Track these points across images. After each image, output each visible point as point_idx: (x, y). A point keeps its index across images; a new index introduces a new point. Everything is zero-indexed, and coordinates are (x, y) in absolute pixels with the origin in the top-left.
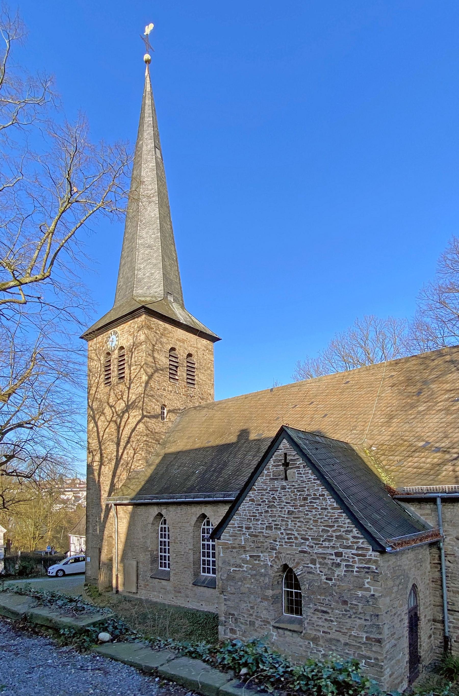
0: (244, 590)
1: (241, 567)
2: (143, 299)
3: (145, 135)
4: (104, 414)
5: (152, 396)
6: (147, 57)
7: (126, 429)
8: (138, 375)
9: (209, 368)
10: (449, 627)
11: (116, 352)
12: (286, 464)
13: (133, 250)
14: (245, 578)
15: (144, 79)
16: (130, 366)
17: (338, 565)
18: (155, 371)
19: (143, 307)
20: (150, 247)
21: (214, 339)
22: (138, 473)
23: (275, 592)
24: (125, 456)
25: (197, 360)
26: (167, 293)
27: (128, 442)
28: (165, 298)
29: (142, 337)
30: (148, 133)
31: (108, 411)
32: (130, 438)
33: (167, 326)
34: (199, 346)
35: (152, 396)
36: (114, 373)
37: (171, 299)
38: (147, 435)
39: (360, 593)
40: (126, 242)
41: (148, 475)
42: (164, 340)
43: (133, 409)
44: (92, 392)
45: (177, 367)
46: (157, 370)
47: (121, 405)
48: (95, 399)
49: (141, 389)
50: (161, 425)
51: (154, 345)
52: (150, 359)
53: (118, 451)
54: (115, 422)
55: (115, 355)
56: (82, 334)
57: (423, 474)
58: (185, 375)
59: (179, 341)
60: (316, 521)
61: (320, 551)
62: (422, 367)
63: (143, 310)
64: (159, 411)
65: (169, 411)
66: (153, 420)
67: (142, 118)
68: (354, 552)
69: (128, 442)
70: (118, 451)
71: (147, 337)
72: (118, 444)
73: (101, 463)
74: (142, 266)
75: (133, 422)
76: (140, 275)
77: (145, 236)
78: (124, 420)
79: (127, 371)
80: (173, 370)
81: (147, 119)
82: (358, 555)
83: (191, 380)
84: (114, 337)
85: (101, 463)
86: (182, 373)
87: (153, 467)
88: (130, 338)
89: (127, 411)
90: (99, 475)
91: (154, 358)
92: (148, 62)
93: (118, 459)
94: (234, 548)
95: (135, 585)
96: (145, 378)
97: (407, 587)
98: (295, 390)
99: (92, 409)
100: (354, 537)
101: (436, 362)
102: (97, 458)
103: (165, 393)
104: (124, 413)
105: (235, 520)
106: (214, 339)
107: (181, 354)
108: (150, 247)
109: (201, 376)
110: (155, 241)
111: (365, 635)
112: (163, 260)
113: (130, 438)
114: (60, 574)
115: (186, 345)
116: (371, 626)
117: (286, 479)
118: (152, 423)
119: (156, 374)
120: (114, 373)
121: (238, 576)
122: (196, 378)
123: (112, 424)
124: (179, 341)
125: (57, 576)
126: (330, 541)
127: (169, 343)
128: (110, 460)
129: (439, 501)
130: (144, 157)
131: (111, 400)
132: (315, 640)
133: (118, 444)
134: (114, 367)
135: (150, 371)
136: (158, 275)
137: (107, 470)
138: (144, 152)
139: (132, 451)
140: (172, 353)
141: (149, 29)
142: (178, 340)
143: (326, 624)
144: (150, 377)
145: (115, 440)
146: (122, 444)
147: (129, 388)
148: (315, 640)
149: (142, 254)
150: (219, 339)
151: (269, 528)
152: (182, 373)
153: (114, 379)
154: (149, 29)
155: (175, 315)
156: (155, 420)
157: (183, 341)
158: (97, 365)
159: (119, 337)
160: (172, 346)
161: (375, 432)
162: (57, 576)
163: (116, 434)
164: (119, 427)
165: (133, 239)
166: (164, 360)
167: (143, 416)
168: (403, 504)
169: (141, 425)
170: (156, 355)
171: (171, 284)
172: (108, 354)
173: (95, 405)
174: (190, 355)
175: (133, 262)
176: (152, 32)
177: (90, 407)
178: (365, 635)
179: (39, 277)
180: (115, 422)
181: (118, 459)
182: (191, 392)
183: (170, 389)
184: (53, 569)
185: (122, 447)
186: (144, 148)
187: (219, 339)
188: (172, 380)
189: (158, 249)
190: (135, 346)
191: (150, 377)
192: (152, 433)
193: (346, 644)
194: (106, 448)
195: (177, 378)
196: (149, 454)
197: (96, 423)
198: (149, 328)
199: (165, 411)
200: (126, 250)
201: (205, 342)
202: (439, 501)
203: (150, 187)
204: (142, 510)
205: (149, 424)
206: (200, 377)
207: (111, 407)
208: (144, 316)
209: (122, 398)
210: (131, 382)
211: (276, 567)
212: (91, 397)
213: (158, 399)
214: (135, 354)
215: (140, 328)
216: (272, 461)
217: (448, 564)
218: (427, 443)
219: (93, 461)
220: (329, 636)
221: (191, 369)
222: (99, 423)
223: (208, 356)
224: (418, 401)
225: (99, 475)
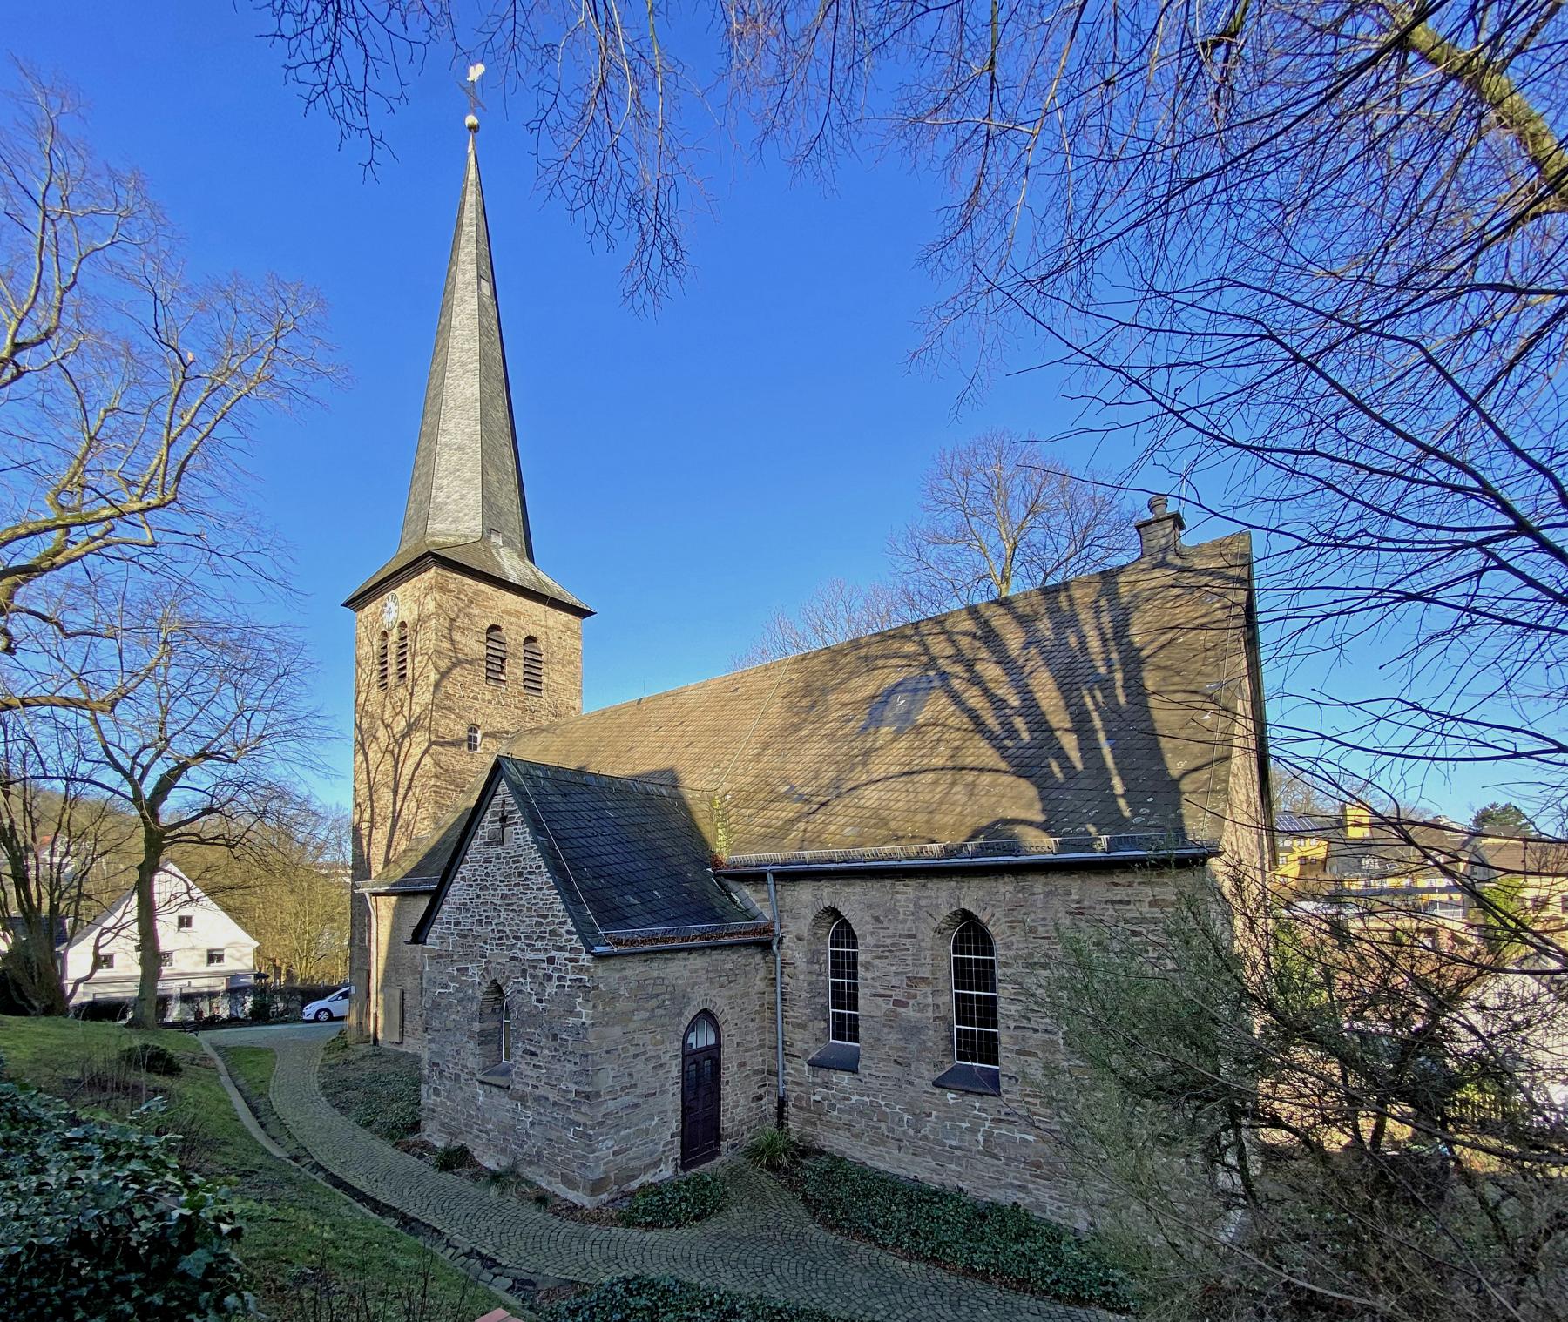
0: (450, 1024)
1: (447, 986)
2: (441, 540)
3: (462, 256)
4: (376, 738)
5: (450, 709)
6: (471, 120)
7: (407, 765)
8: (424, 670)
9: (572, 663)
10: (784, 1082)
11: (395, 630)
12: (503, 819)
13: (432, 452)
14: (451, 1005)
15: (467, 156)
16: (413, 656)
17: (550, 978)
18: (455, 665)
19: (429, 554)
20: (461, 448)
21: (582, 613)
22: (420, 840)
23: (485, 1025)
24: (405, 812)
25: (548, 647)
26: (489, 530)
27: (409, 788)
28: (485, 538)
29: (431, 606)
30: (468, 251)
31: (382, 733)
32: (411, 780)
33: (483, 587)
34: (551, 623)
35: (450, 709)
36: (392, 669)
37: (497, 540)
38: (436, 776)
39: (571, 1021)
40: (423, 440)
41: (432, 843)
42: (475, 611)
43: (417, 730)
44: (361, 700)
45: (503, 660)
46: (457, 663)
47: (400, 725)
48: (365, 713)
49: (427, 697)
50: (468, 759)
51: (453, 620)
52: (446, 645)
53: (395, 803)
54: (392, 752)
55: (394, 636)
56: (346, 599)
57: (775, 835)
58: (520, 673)
59: (509, 613)
60: (529, 909)
61: (532, 956)
62: (829, 666)
63: (430, 559)
64: (463, 734)
65: (485, 735)
66: (452, 750)
67: (459, 226)
68: (567, 955)
69: (409, 788)
70: (395, 803)
71: (439, 606)
72: (395, 792)
73: (372, 826)
74: (445, 482)
75: (417, 752)
76: (440, 497)
77: (453, 430)
78: (404, 749)
79: (409, 664)
80: (495, 667)
81: (466, 229)
82: (570, 960)
83: (532, 682)
84: (391, 604)
85: (372, 826)
86: (514, 670)
87: (442, 831)
88: (415, 607)
89: (408, 734)
90: (369, 844)
91: (452, 642)
92: (474, 128)
93: (396, 818)
94: (440, 957)
95: (398, 1030)
96: (434, 676)
97: (680, 1014)
98: (669, 700)
99: (361, 732)
100: (568, 932)
101: (849, 658)
102: (367, 816)
103: (476, 704)
104: (403, 737)
105: (444, 914)
106: (582, 613)
107: (513, 636)
108: (461, 448)
109: (555, 676)
110: (470, 439)
111: (573, 1088)
112: (484, 472)
113: (411, 780)
114: (324, 1016)
115: (522, 623)
116: (581, 1073)
117: (502, 843)
118: (448, 756)
119: (458, 670)
120: (392, 669)
121: (443, 1002)
122: (544, 678)
123: (388, 757)
124: (509, 613)
125: (316, 1020)
126: (543, 939)
127: (486, 617)
128: (385, 819)
129: (770, 877)
130: (458, 294)
131: (387, 715)
132: (523, 1099)
133: (395, 792)
134: (392, 658)
135: (444, 664)
136: (474, 498)
137: (380, 836)
138: (459, 285)
139: (414, 804)
140: (493, 635)
141: (476, 72)
142: (504, 611)
143: (534, 1073)
144: (444, 675)
145: (392, 784)
146: (401, 791)
147: (411, 694)
148: (523, 1099)
149: (445, 461)
150: (589, 613)
151: (480, 922)
152: (514, 670)
153: (392, 680)
154: (476, 72)
155: (500, 567)
156: (454, 750)
157: (517, 614)
158: (369, 650)
159: (400, 605)
160: (492, 622)
161: (740, 771)
162: (316, 1020)
163: (392, 774)
164: (397, 763)
165: (432, 437)
166: (474, 645)
167: (431, 743)
168: (732, 884)
169: (427, 760)
170: (457, 636)
171: (500, 514)
172: (385, 634)
173: (365, 724)
174: (531, 639)
175: (430, 474)
176: (481, 77)
177: (358, 727)
178: (573, 1088)
179: (154, 502)
180: (392, 752)
181: (396, 818)
182: (533, 701)
183: (488, 696)
184: (311, 1010)
185: (400, 797)
186: (459, 278)
187: (589, 613)
188: (492, 682)
189: (475, 452)
190: (422, 620)
191: (444, 675)
192: (445, 772)
193: (555, 1104)
194: (379, 798)
195: (502, 677)
196: (441, 809)
197: (366, 755)
198: (443, 589)
199: (479, 735)
200: (422, 454)
201: (564, 617)
202: (770, 877)
203: (466, 346)
204: (410, 901)
205: (442, 758)
206: (551, 676)
207: (386, 726)
208: (434, 569)
209: (401, 712)
210: (414, 684)
211: (484, 985)
212: (360, 709)
213: (463, 713)
214: (421, 635)
215: (429, 590)
216: (488, 816)
217: (787, 979)
218: (792, 787)
219: (360, 822)
220: (537, 1092)
221: (532, 663)
222: (371, 755)
223: (570, 642)
224: (805, 720)
225: (369, 844)
